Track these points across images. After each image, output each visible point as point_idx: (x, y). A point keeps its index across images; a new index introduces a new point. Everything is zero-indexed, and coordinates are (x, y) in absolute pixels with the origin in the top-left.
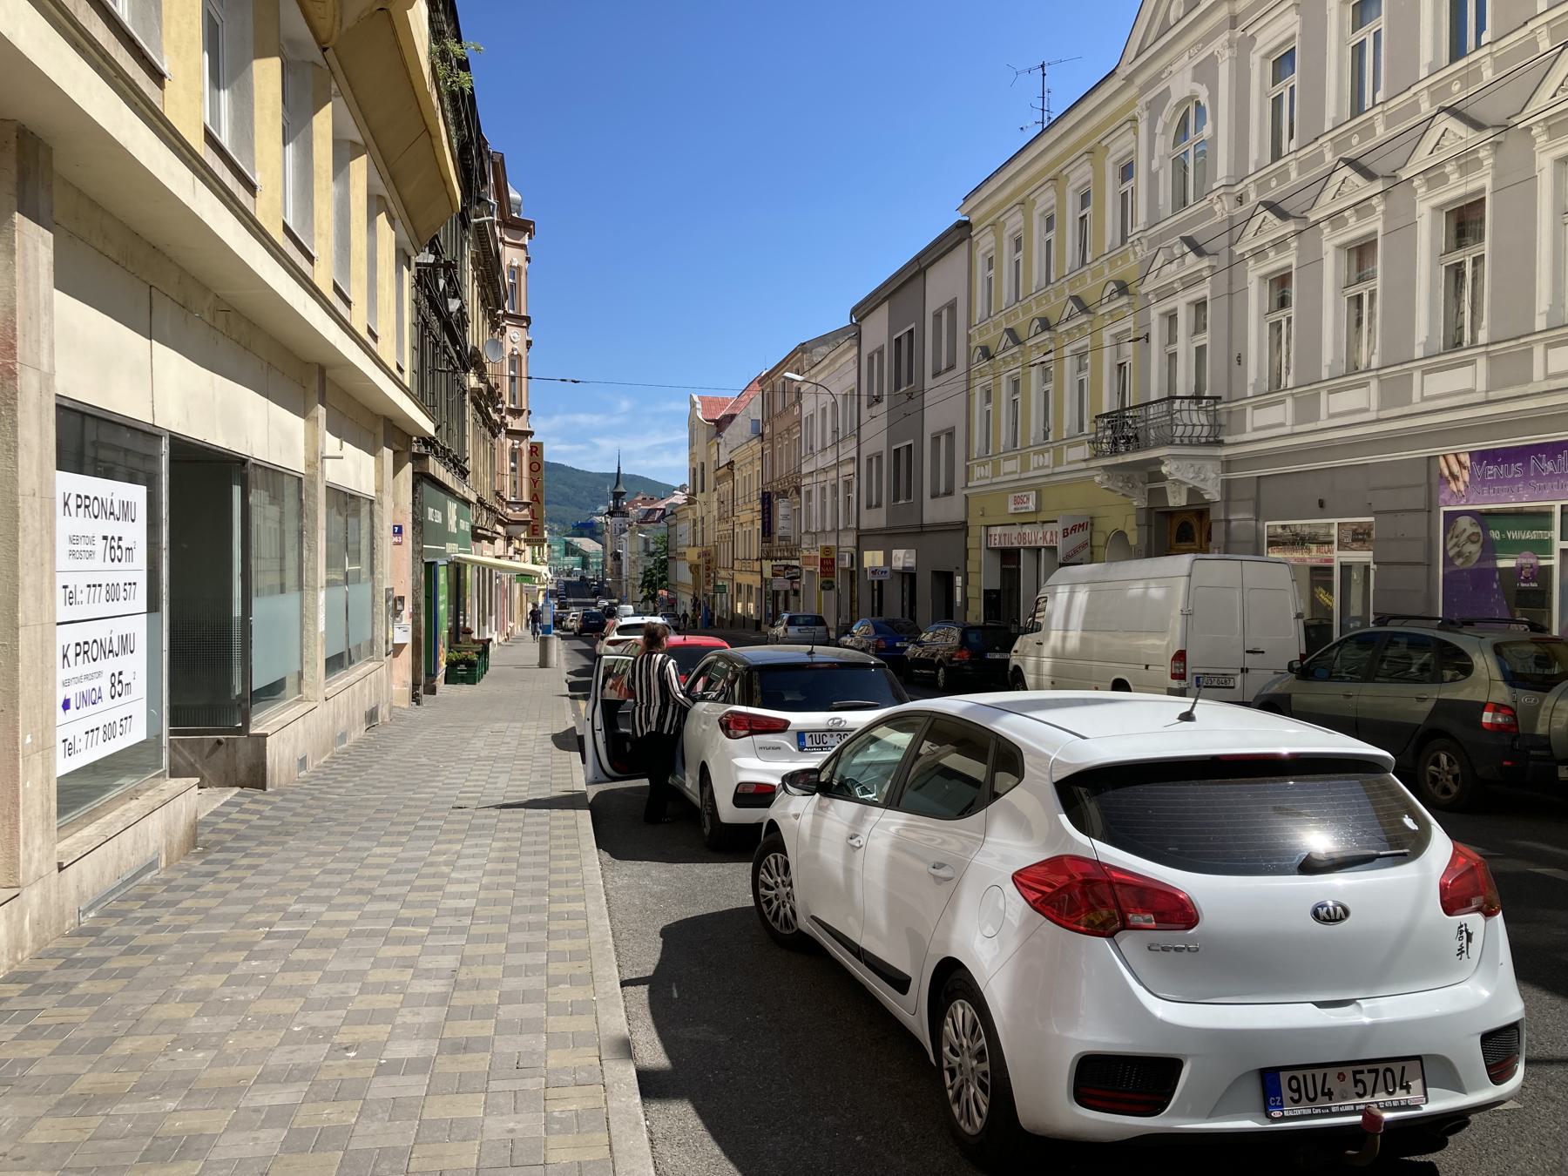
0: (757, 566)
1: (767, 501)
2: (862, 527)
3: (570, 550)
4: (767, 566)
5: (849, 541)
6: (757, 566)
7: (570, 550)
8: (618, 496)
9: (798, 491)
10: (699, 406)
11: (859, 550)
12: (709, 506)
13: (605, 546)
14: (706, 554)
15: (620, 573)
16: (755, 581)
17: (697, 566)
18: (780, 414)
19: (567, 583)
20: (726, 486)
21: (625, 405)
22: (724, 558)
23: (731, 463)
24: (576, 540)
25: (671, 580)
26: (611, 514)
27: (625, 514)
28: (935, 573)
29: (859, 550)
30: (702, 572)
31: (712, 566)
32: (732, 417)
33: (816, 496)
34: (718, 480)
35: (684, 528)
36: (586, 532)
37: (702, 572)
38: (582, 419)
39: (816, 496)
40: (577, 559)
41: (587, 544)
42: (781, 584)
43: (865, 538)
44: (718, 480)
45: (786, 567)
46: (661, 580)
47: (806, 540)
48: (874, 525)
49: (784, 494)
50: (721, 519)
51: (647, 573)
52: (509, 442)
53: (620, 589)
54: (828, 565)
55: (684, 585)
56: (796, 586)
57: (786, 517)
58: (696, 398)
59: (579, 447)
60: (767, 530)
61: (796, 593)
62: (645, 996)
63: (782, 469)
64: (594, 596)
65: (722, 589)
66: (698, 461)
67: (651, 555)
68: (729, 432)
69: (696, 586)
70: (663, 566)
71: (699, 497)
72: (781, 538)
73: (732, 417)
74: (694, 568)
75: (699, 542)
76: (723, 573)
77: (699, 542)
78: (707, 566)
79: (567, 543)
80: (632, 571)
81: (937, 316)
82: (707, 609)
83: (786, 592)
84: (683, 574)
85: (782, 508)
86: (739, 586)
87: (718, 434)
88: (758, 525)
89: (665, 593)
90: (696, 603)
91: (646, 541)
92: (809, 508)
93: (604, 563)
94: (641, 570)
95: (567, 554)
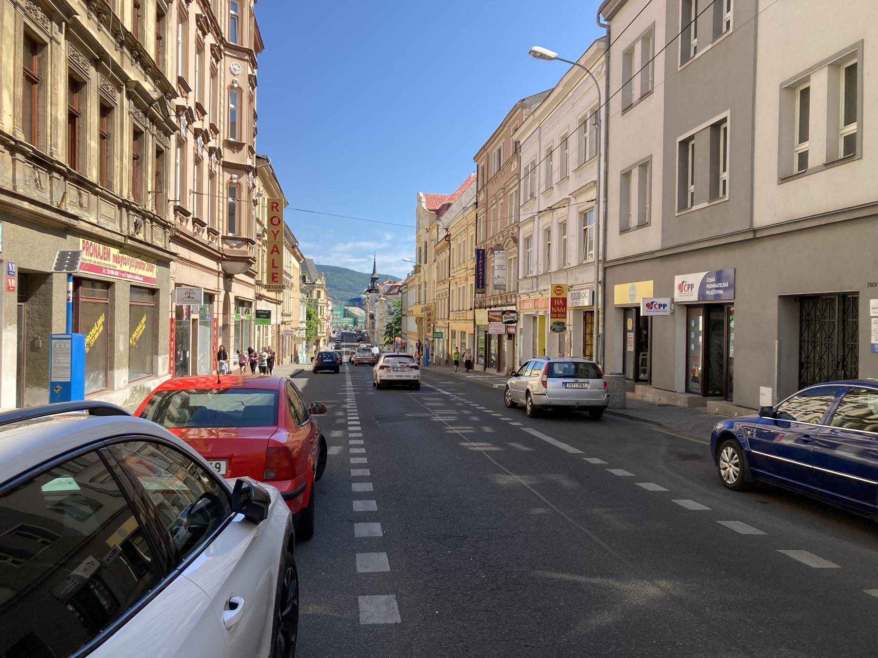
0: (470, 315)
1: (481, 256)
2: (610, 256)
3: (346, 314)
4: (482, 316)
5: (590, 276)
6: (470, 315)
7: (346, 314)
8: (374, 280)
9: (516, 241)
10: (424, 200)
11: (605, 285)
12: (431, 273)
13: (366, 312)
14: (427, 309)
15: (373, 327)
16: (469, 328)
17: (421, 319)
18: (495, 177)
19: (343, 334)
20: (445, 255)
21: (388, 237)
22: (441, 312)
23: (448, 236)
24: (350, 308)
25: (404, 330)
26: (369, 291)
27: (377, 291)
28: (785, 299)
29: (605, 285)
30: (425, 323)
31: (432, 318)
32: (449, 205)
33: (538, 243)
34: (438, 252)
35: (412, 295)
36: (357, 304)
37: (425, 323)
38: (364, 244)
39: (538, 243)
40: (351, 320)
41: (356, 311)
42: (496, 328)
43: (610, 270)
44: (438, 252)
45: (504, 312)
46: (397, 330)
47: (524, 287)
48: (373, 556)
49: (499, 247)
50: (440, 282)
51: (389, 326)
52: (227, 176)
53: (373, 338)
54: (559, 306)
55: (412, 333)
56: (512, 330)
57: (501, 267)
58: (421, 194)
59: (362, 260)
60: (481, 282)
61: (511, 336)
62: (391, 621)
63: (496, 227)
64: (358, 341)
65: (439, 335)
66: (423, 240)
67: (392, 314)
68: (446, 218)
69: (420, 333)
70: (399, 321)
71: (424, 267)
72: (496, 287)
73: (449, 205)
74: (419, 321)
75: (422, 299)
76: (440, 323)
77: (422, 299)
78: (428, 319)
79: (345, 310)
80: (380, 326)
81: (626, 175)
82: (428, 350)
83: (500, 337)
84: (411, 325)
85: (496, 261)
86: (454, 333)
87: (438, 219)
88: (472, 280)
89: (400, 339)
90: (419, 346)
91: (389, 307)
92: (528, 256)
93: (366, 322)
94: (386, 324)
95: (345, 316)
